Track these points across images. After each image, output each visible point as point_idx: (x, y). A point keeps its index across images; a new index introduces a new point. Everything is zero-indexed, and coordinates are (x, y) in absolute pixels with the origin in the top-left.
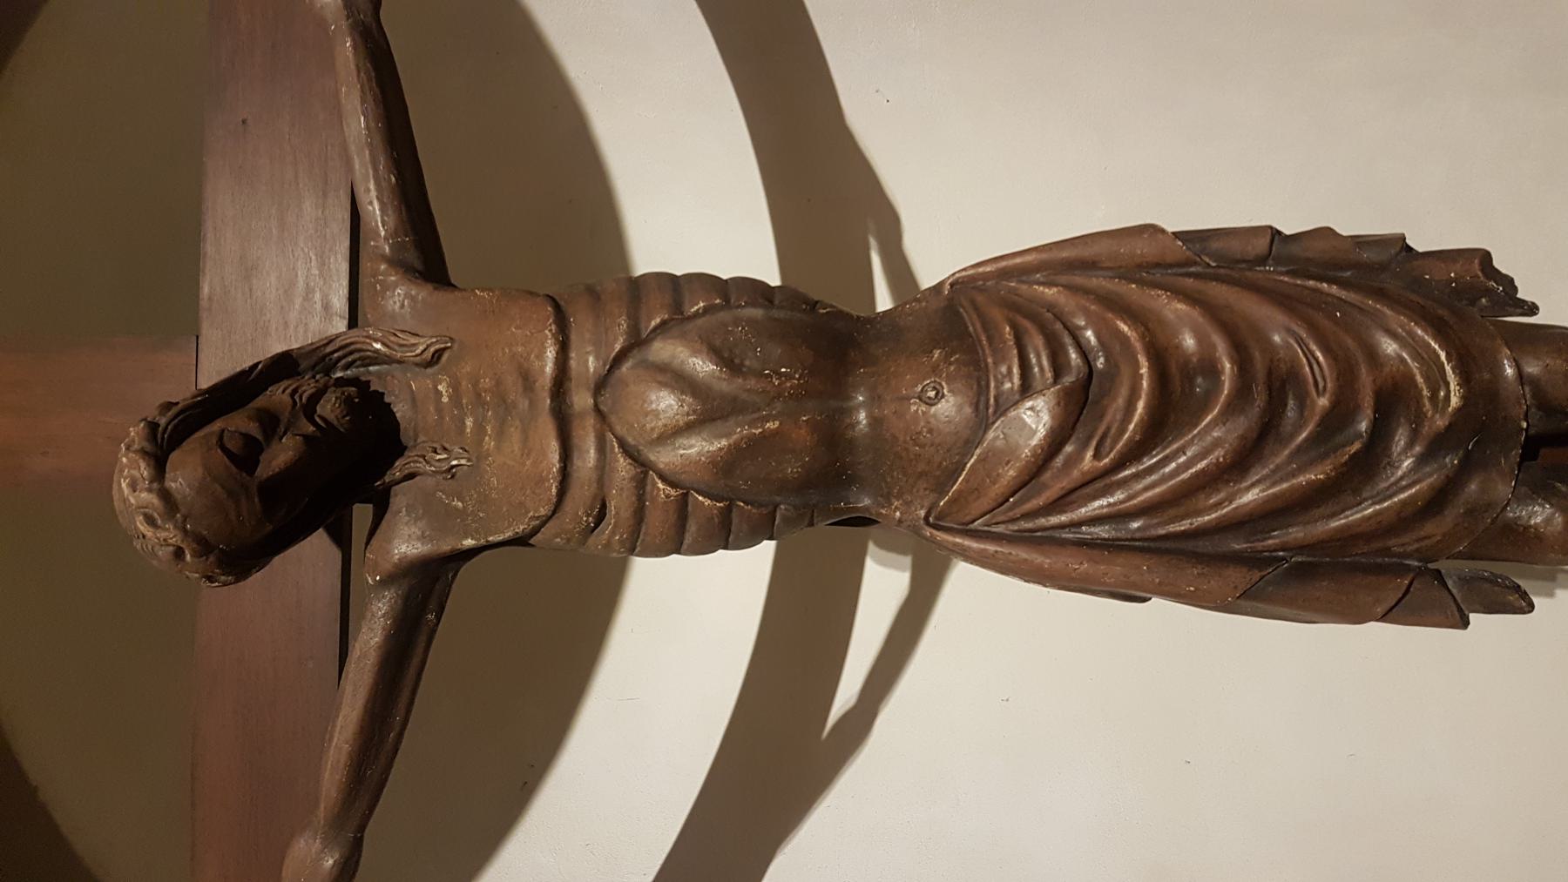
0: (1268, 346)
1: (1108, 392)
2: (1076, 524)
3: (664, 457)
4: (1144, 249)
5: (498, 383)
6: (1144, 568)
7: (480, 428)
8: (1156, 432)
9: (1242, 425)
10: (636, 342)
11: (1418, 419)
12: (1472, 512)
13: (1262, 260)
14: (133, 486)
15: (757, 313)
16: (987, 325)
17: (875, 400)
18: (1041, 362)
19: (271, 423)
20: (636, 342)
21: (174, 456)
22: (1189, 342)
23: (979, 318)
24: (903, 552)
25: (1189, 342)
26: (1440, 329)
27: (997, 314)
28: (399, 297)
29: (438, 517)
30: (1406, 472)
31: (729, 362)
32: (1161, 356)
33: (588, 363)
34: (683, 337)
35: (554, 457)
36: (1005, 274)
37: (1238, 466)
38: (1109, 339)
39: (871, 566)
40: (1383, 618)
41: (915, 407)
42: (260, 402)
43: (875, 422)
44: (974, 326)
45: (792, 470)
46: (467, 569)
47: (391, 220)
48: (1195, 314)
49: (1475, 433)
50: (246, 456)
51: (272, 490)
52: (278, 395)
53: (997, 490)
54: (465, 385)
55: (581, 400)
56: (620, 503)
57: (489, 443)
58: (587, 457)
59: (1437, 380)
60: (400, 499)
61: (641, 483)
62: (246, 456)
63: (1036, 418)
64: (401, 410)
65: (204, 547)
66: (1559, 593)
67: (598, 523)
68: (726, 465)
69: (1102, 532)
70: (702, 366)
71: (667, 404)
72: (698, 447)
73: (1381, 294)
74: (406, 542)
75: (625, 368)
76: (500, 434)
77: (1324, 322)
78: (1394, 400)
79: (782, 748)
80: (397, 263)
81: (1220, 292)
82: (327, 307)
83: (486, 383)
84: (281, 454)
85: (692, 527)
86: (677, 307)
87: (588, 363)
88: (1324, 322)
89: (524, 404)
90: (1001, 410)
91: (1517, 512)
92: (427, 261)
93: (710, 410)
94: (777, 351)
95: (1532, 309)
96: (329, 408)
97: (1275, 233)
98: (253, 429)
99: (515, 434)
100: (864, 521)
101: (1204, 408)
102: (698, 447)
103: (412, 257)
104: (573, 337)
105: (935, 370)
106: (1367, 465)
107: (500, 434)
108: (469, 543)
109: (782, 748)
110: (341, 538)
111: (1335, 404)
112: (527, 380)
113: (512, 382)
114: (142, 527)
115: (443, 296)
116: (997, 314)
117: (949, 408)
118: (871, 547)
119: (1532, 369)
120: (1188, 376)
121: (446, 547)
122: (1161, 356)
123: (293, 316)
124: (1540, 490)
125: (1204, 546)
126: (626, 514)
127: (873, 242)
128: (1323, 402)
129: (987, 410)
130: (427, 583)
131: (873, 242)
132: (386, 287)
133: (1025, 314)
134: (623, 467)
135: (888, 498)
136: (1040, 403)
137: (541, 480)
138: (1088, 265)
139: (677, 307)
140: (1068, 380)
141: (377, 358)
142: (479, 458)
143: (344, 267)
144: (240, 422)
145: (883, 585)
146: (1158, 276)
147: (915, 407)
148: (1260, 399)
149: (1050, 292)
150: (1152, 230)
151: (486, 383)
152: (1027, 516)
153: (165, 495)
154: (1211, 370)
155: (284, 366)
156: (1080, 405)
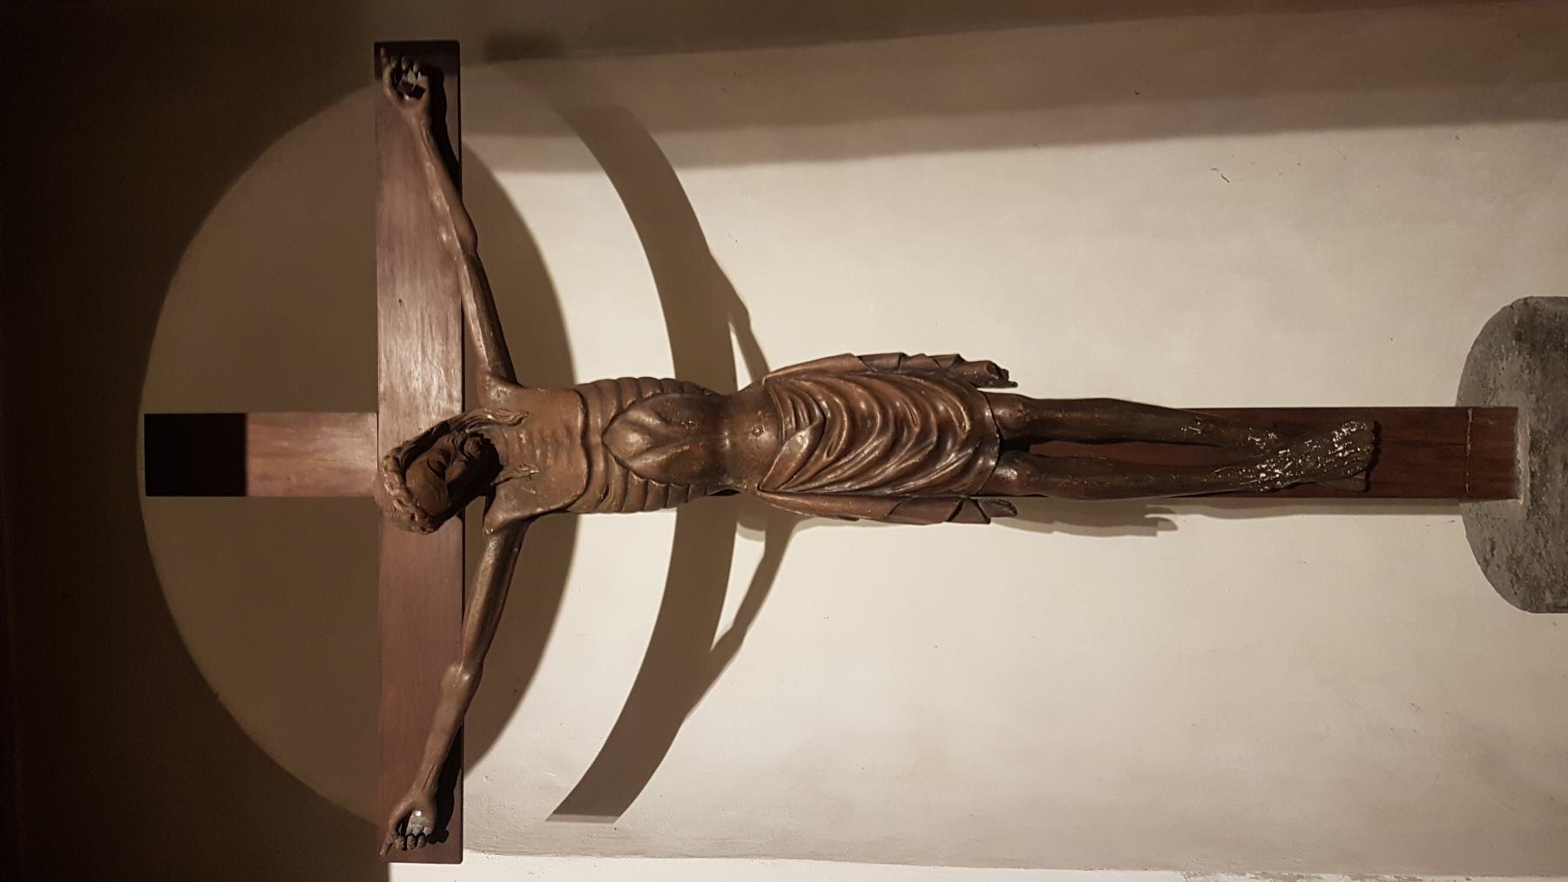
0: (894, 407)
1: (831, 429)
2: (823, 486)
3: (637, 464)
4: (846, 363)
5: (553, 433)
6: (851, 505)
7: (544, 455)
8: (853, 443)
9: (885, 440)
10: (621, 411)
11: (955, 435)
12: (981, 472)
13: (896, 368)
14: (391, 487)
15: (677, 396)
16: (781, 400)
17: (733, 434)
18: (804, 416)
19: (446, 454)
20: (621, 411)
21: (408, 472)
22: (863, 406)
23: (780, 394)
24: (758, 528)
25: (863, 406)
26: (962, 398)
27: (785, 394)
28: (498, 393)
29: (525, 500)
30: (952, 460)
31: (665, 420)
32: (852, 412)
33: (597, 421)
34: (644, 409)
35: (585, 466)
36: (796, 374)
37: (885, 456)
38: (831, 405)
39: (738, 538)
40: (950, 520)
41: (751, 437)
42: (437, 445)
43: (733, 444)
44: (775, 400)
45: (696, 468)
46: (532, 526)
47: (492, 354)
48: (866, 393)
49: (979, 438)
50: (441, 471)
51: (452, 487)
52: (445, 441)
53: (787, 474)
54: (536, 434)
55: (595, 439)
56: (616, 486)
57: (550, 461)
58: (600, 466)
59: (961, 420)
60: (502, 492)
61: (626, 477)
62: (441, 471)
63: (803, 438)
64: (499, 448)
65: (424, 514)
66: (1160, 533)
67: (606, 495)
68: (665, 467)
69: (835, 489)
70: (650, 421)
71: (634, 438)
72: (651, 460)
73: (941, 383)
74: (502, 513)
75: (616, 424)
76: (556, 456)
77: (916, 395)
78: (945, 427)
79: (685, 657)
80: (494, 375)
81: (877, 384)
82: (450, 396)
83: (547, 432)
84: (455, 470)
85: (650, 497)
86: (639, 394)
87: (597, 421)
88: (916, 395)
89: (567, 442)
90: (788, 437)
91: (1001, 472)
92: (508, 375)
93: (656, 442)
94: (687, 413)
95: (1014, 385)
96: (470, 447)
97: (902, 356)
98: (441, 459)
99: (564, 458)
100: (730, 492)
101: (870, 434)
102: (651, 460)
103: (502, 372)
104: (591, 410)
105: (759, 420)
106: (938, 453)
107: (556, 456)
108: (540, 510)
109: (685, 657)
110: (462, 517)
111: (922, 430)
112: (569, 431)
113: (562, 432)
114: (396, 505)
115: (520, 391)
116: (785, 394)
117: (766, 436)
118: (739, 526)
119: (1000, 412)
120: (864, 421)
121: (527, 513)
122: (852, 412)
123: (432, 401)
124: (1010, 463)
125: (876, 492)
126: (619, 491)
127: (732, 327)
128: (917, 430)
129: (782, 437)
130: (514, 533)
131: (732, 327)
132: (491, 388)
133: (796, 393)
134: (617, 469)
135: (740, 480)
136: (803, 433)
137: (579, 477)
138: (823, 372)
139: (639, 394)
140: (816, 423)
141: (488, 422)
142: (544, 469)
143: (459, 375)
144: (433, 455)
145: (747, 550)
146: (853, 377)
147: (751, 437)
148: (892, 425)
149: (807, 384)
150: (849, 356)
151: (547, 432)
152: (802, 483)
153: (408, 490)
154: (873, 418)
155: (444, 428)
156: (821, 433)
